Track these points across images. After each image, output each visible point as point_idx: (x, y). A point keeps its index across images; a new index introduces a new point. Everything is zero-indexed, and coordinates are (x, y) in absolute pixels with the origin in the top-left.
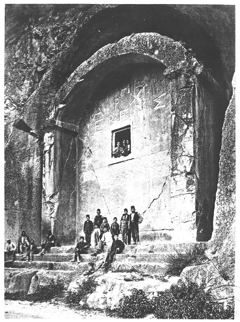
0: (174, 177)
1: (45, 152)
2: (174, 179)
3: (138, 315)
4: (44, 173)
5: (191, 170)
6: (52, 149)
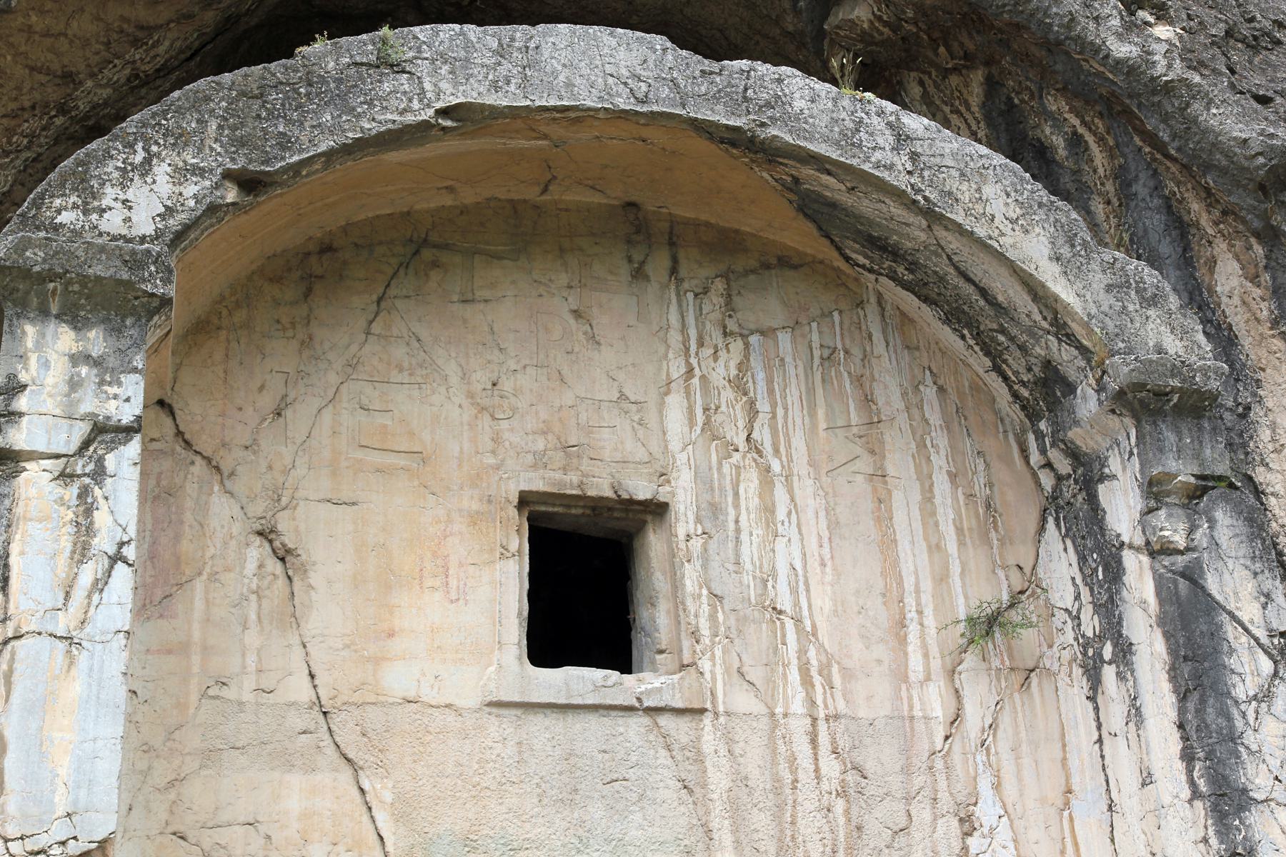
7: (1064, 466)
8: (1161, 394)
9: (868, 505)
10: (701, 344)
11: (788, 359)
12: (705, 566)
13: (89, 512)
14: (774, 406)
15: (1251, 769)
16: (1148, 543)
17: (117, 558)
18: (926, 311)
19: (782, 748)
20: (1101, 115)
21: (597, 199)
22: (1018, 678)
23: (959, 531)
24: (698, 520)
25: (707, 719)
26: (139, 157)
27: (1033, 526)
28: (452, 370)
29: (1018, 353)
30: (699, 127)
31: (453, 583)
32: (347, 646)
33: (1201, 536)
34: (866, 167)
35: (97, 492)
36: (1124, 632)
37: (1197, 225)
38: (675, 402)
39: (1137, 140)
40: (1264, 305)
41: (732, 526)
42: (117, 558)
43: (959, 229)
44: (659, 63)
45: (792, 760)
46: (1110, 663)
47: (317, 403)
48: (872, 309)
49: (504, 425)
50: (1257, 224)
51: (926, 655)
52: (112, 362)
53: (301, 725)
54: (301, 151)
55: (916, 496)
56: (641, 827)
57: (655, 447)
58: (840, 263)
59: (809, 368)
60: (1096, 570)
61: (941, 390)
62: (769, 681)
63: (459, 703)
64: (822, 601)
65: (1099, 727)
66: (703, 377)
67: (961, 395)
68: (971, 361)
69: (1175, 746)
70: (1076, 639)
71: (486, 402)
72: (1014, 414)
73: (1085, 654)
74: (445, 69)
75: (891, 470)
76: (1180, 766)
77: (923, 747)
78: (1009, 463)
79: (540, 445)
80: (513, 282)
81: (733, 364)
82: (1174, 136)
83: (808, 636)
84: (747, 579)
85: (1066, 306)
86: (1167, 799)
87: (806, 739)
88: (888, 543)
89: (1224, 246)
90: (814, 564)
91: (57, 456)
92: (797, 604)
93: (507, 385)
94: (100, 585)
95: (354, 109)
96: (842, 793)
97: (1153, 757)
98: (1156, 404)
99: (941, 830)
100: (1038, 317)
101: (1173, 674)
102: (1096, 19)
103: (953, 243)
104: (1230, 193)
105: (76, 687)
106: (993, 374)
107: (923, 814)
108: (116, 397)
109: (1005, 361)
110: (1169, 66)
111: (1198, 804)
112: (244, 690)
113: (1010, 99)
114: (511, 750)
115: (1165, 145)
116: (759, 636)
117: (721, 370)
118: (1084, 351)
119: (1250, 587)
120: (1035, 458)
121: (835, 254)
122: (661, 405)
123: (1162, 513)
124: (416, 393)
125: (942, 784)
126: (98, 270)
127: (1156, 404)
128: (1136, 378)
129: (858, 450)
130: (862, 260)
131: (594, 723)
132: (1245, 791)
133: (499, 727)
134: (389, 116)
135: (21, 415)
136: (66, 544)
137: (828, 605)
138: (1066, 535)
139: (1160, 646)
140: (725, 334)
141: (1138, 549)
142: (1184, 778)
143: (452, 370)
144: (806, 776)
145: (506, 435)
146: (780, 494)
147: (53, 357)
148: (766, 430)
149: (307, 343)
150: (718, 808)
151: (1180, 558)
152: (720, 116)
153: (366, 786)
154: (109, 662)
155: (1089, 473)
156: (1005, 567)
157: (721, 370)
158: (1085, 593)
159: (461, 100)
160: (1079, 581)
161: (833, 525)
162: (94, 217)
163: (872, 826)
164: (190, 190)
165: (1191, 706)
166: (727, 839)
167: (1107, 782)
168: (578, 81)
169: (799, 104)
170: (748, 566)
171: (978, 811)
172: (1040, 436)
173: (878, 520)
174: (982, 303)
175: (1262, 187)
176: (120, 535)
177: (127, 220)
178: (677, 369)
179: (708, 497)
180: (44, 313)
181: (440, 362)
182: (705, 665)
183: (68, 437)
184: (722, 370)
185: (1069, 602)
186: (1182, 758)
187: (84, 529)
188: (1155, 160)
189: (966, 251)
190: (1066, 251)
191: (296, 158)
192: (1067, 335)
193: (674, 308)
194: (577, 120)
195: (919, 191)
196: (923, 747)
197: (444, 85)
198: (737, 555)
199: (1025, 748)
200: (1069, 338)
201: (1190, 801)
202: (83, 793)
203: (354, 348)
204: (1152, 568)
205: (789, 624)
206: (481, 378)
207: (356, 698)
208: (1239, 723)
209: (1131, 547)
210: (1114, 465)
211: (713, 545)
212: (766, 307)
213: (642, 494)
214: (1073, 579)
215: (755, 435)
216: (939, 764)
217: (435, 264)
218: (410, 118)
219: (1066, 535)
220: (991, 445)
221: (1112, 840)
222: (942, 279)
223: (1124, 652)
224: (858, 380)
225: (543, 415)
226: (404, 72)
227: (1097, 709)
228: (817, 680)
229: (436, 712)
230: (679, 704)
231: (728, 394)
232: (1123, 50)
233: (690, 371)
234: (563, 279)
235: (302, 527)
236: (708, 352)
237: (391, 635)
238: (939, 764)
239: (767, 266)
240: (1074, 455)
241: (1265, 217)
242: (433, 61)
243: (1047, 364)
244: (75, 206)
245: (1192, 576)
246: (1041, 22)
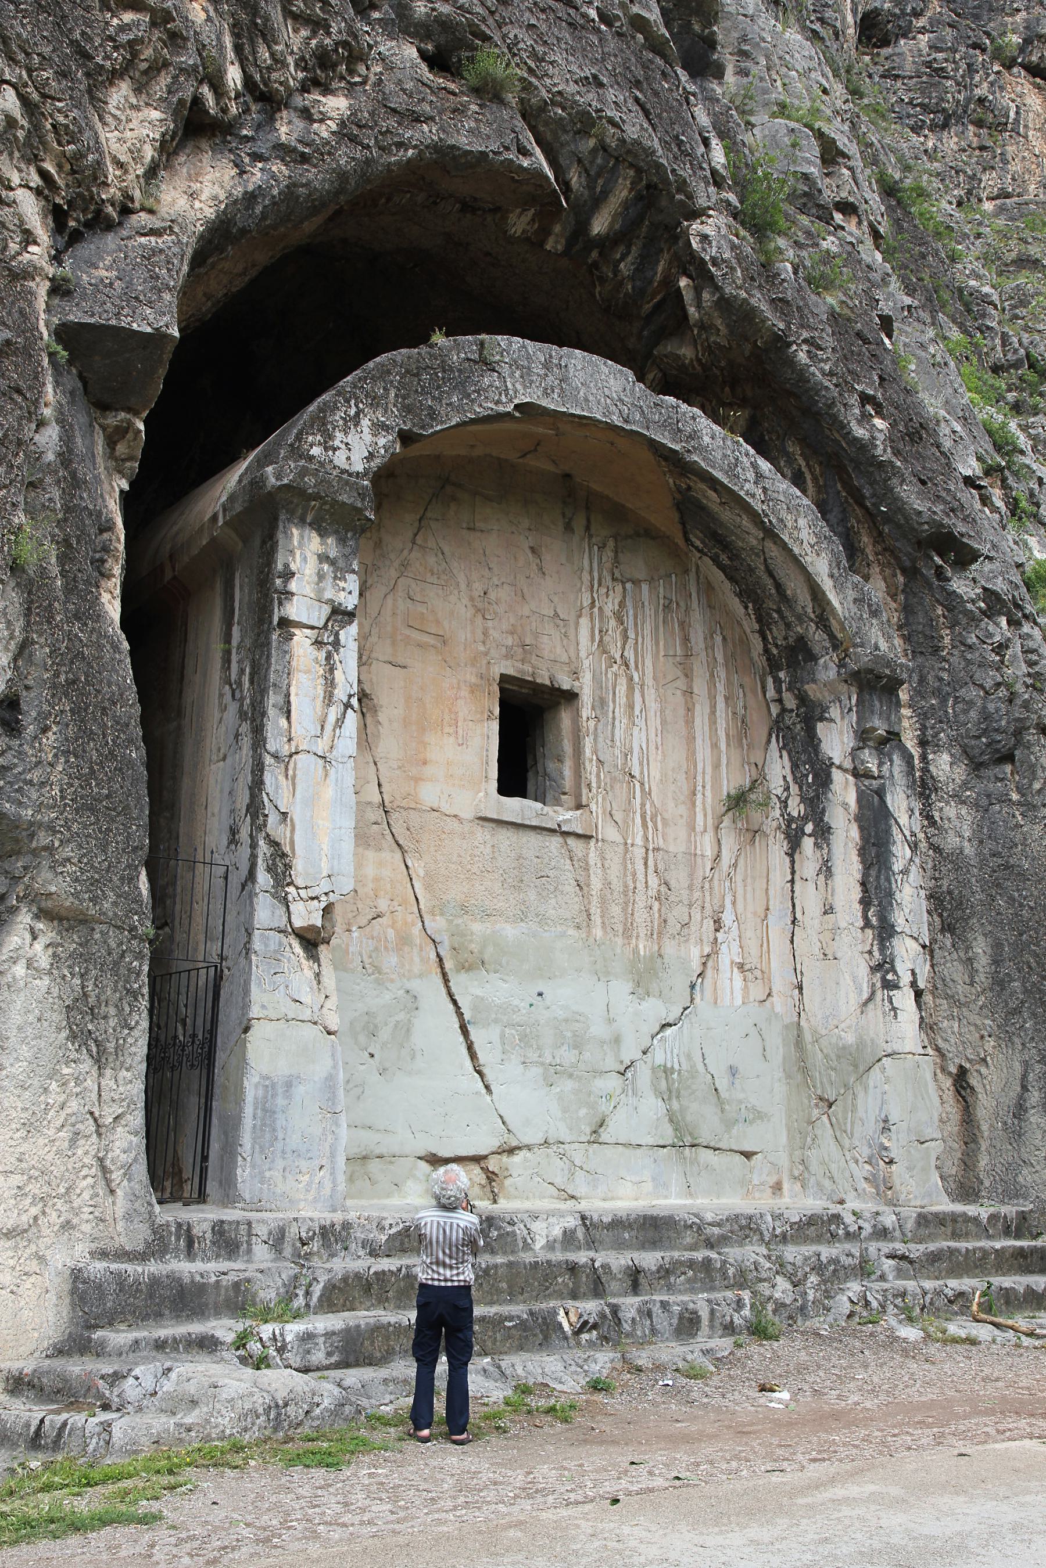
7: (790, 702)
8: (879, 677)
9: (682, 711)
10: (600, 585)
11: (646, 603)
12: (595, 740)
13: (332, 670)
14: (637, 635)
16: (855, 768)
17: (348, 706)
18: (727, 584)
19: (629, 866)
20: (821, 464)
21: (552, 468)
22: (749, 835)
23: (727, 735)
24: (593, 708)
25: (593, 842)
26: (352, 411)
27: (764, 739)
28: (462, 579)
29: (783, 627)
30: (652, 444)
31: (460, 732)
32: (399, 768)
33: (886, 767)
34: (742, 493)
35: (336, 657)
36: (826, 819)
37: (863, 551)
38: (584, 622)
39: (839, 486)
40: (896, 614)
41: (611, 715)
42: (348, 706)
43: (784, 546)
44: (633, 391)
45: (634, 874)
46: (810, 836)
47: (384, 590)
48: (693, 574)
49: (490, 624)
50: (908, 564)
51: (705, 815)
52: (341, 563)
53: (373, 819)
54: (442, 423)
55: (707, 710)
56: (554, 908)
57: (573, 655)
58: (680, 541)
59: (657, 612)
60: (807, 776)
61: (724, 639)
62: (625, 822)
63: (462, 815)
64: (655, 772)
65: (793, 873)
66: (600, 608)
67: (734, 643)
68: (744, 622)
69: (857, 893)
70: (782, 815)
71: (480, 605)
72: (761, 662)
73: (789, 826)
74: (518, 374)
75: (696, 691)
76: (858, 908)
77: (700, 874)
78: (756, 695)
79: (509, 641)
80: (498, 520)
81: (617, 601)
82: (874, 495)
83: (646, 794)
84: (617, 752)
85: (833, 609)
86: (843, 924)
87: (642, 862)
88: (691, 739)
89: (877, 570)
90: (652, 747)
91: (312, 628)
92: (642, 773)
93: (492, 595)
94: (340, 722)
95: (469, 395)
96: (658, 899)
97: (836, 897)
98: (875, 684)
99: (705, 927)
100: (809, 610)
101: (862, 852)
102: (845, 405)
103: (773, 551)
104: (897, 540)
105: (329, 792)
106: (757, 635)
107: (697, 916)
108: (344, 589)
109: (770, 630)
110: (885, 451)
111: (869, 932)
113: (762, 436)
114: (488, 850)
115: (863, 497)
116: (621, 791)
118: (832, 637)
119: (904, 805)
120: (771, 693)
121: (681, 535)
122: (577, 624)
123: (867, 751)
124: (440, 592)
125: (708, 898)
126: (344, 498)
127: (875, 684)
128: (871, 666)
129: (679, 674)
130: (698, 543)
131: (533, 840)
132: (893, 926)
133: (483, 834)
134: (490, 405)
135: (293, 594)
136: (320, 691)
137: (658, 776)
138: (784, 747)
139: (855, 833)
140: (614, 579)
141: (845, 771)
142: (860, 914)
143: (462, 579)
144: (640, 886)
145: (491, 631)
147: (309, 555)
148: (632, 652)
149: (378, 544)
150: (595, 901)
151: (874, 782)
152: (664, 439)
153: (410, 864)
154: (345, 774)
155: (811, 713)
156: (749, 764)
157: (610, 605)
158: (794, 789)
159: (528, 400)
160: (789, 778)
161: (664, 722)
162: (330, 453)
163: (671, 921)
164: (382, 442)
165: (873, 872)
166: (599, 921)
167: (794, 906)
168: (591, 398)
169: (707, 439)
170: (618, 744)
171: (723, 916)
172: (777, 681)
173: (687, 722)
174: (773, 591)
175: (919, 543)
176: (349, 690)
177: (348, 458)
179: (598, 692)
180: (302, 521)
181: (455, 571)
182: (593, 807)
183: (318, 615)
184: (610, 605)
185: (779, 791)
186: (861, 902)
187: (330, 683)
188: (847, 501)
189: (780, 559)
190: (835, 571)
191: (439, 428)
192: (825, 626)
194: (586, 425)
195: (767, 515)
197: (519, 386)
198: (613, 735)
199: (749, 880)
200: (827, 629)
201: (862, 929)
202: (336, 862)
203: (406, 552)
204: (856, 785)
205: (638, 785)
206: (478, 588)
207: (404, 804)
209: (839, 767)
210: (834, 712)
211: (600, 726)
212: (636, 565)
213: (565, 687)
214: (784, 777)
215: (626, 654)
216: (707, 886)
217: (454, 498)
218: (501, 409)
219: (784, 747)
220: (747, 680)
221: (792, 942)
222: (751, 570)
223: (823, 832)
224: (682, 624)
225: (512, 621)
226: (494, 370)
227: (793, 862)
228: (650, 824)
229: (448, 819)
230: (580, 832)
231: (613, 623)
232: (860, 432)
233: (593, 602)
234: (526, 523)
235: (374, 680)
236: (604, 590)
237: (425, 763)
238: (707, 886)
239: (638, 535)
240: (803, 699)
241: (914, 561)
242: (511, 366)
243: (801, 639)
244: (320, 444)
245: (880, 793)
246: (812, 397)
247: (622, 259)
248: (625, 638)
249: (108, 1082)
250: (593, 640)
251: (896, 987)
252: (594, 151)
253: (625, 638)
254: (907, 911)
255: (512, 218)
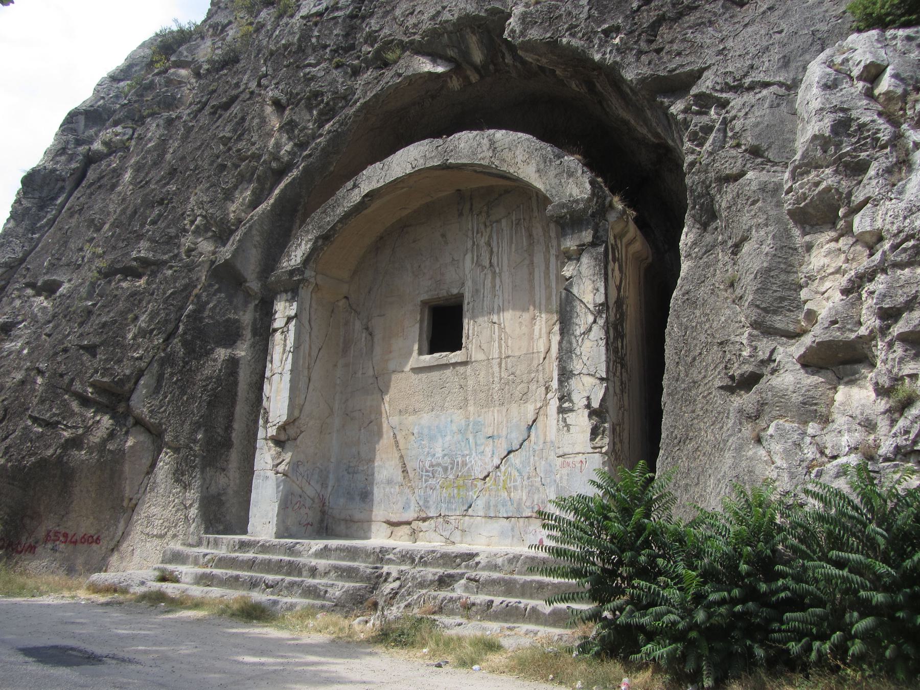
0: (565, 416)
1: (275, 330)
2: (565, 420)
3: (217, 55)
4: (268, 374)
5: (601, 405)
6: (292, 326)
10: (477, 233)
15: (575, 362)
55: (543, 268)
112: (359, 374)
117: (483, 240)
146: (498, 280)
178: (470, 243)
187: (285, 345)
193: (470, 224)
196: (535, 363)
208: (575, 345)
239: (500, 195)
247: (504, 59)
248: (491, 252)
249: (188, 494)
250: (473, 262)
251: (571, 410)
252: (449, 37)
253: (491, 252)
254: (585, 359)
255: (450, 85)
